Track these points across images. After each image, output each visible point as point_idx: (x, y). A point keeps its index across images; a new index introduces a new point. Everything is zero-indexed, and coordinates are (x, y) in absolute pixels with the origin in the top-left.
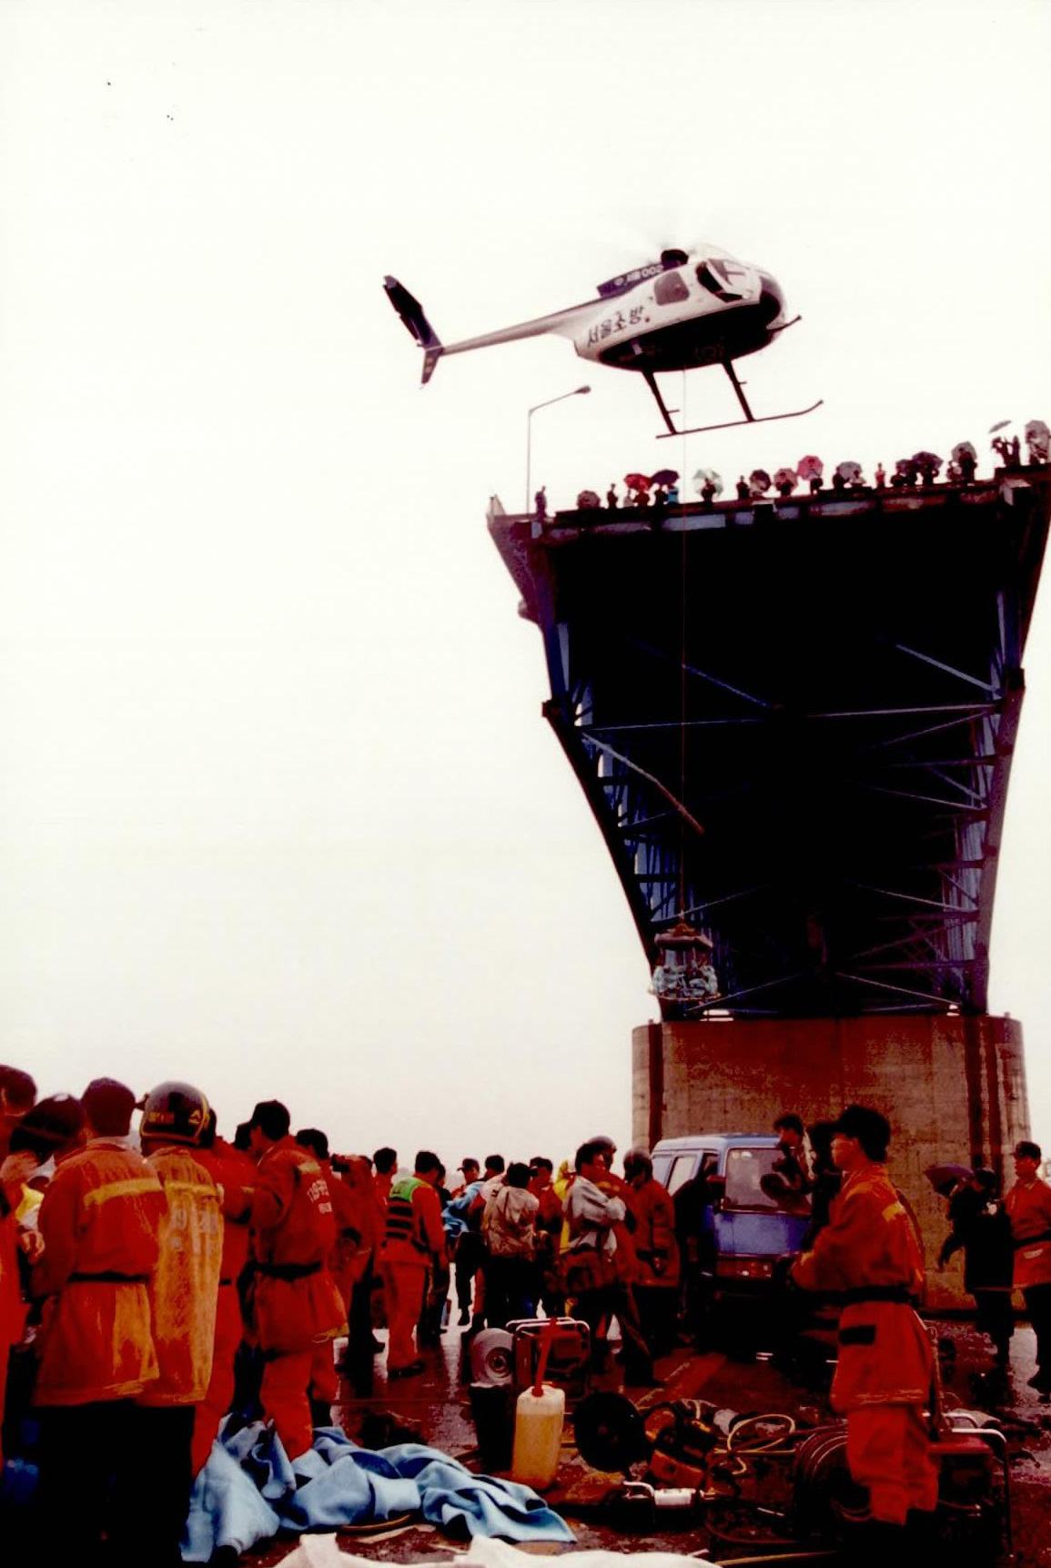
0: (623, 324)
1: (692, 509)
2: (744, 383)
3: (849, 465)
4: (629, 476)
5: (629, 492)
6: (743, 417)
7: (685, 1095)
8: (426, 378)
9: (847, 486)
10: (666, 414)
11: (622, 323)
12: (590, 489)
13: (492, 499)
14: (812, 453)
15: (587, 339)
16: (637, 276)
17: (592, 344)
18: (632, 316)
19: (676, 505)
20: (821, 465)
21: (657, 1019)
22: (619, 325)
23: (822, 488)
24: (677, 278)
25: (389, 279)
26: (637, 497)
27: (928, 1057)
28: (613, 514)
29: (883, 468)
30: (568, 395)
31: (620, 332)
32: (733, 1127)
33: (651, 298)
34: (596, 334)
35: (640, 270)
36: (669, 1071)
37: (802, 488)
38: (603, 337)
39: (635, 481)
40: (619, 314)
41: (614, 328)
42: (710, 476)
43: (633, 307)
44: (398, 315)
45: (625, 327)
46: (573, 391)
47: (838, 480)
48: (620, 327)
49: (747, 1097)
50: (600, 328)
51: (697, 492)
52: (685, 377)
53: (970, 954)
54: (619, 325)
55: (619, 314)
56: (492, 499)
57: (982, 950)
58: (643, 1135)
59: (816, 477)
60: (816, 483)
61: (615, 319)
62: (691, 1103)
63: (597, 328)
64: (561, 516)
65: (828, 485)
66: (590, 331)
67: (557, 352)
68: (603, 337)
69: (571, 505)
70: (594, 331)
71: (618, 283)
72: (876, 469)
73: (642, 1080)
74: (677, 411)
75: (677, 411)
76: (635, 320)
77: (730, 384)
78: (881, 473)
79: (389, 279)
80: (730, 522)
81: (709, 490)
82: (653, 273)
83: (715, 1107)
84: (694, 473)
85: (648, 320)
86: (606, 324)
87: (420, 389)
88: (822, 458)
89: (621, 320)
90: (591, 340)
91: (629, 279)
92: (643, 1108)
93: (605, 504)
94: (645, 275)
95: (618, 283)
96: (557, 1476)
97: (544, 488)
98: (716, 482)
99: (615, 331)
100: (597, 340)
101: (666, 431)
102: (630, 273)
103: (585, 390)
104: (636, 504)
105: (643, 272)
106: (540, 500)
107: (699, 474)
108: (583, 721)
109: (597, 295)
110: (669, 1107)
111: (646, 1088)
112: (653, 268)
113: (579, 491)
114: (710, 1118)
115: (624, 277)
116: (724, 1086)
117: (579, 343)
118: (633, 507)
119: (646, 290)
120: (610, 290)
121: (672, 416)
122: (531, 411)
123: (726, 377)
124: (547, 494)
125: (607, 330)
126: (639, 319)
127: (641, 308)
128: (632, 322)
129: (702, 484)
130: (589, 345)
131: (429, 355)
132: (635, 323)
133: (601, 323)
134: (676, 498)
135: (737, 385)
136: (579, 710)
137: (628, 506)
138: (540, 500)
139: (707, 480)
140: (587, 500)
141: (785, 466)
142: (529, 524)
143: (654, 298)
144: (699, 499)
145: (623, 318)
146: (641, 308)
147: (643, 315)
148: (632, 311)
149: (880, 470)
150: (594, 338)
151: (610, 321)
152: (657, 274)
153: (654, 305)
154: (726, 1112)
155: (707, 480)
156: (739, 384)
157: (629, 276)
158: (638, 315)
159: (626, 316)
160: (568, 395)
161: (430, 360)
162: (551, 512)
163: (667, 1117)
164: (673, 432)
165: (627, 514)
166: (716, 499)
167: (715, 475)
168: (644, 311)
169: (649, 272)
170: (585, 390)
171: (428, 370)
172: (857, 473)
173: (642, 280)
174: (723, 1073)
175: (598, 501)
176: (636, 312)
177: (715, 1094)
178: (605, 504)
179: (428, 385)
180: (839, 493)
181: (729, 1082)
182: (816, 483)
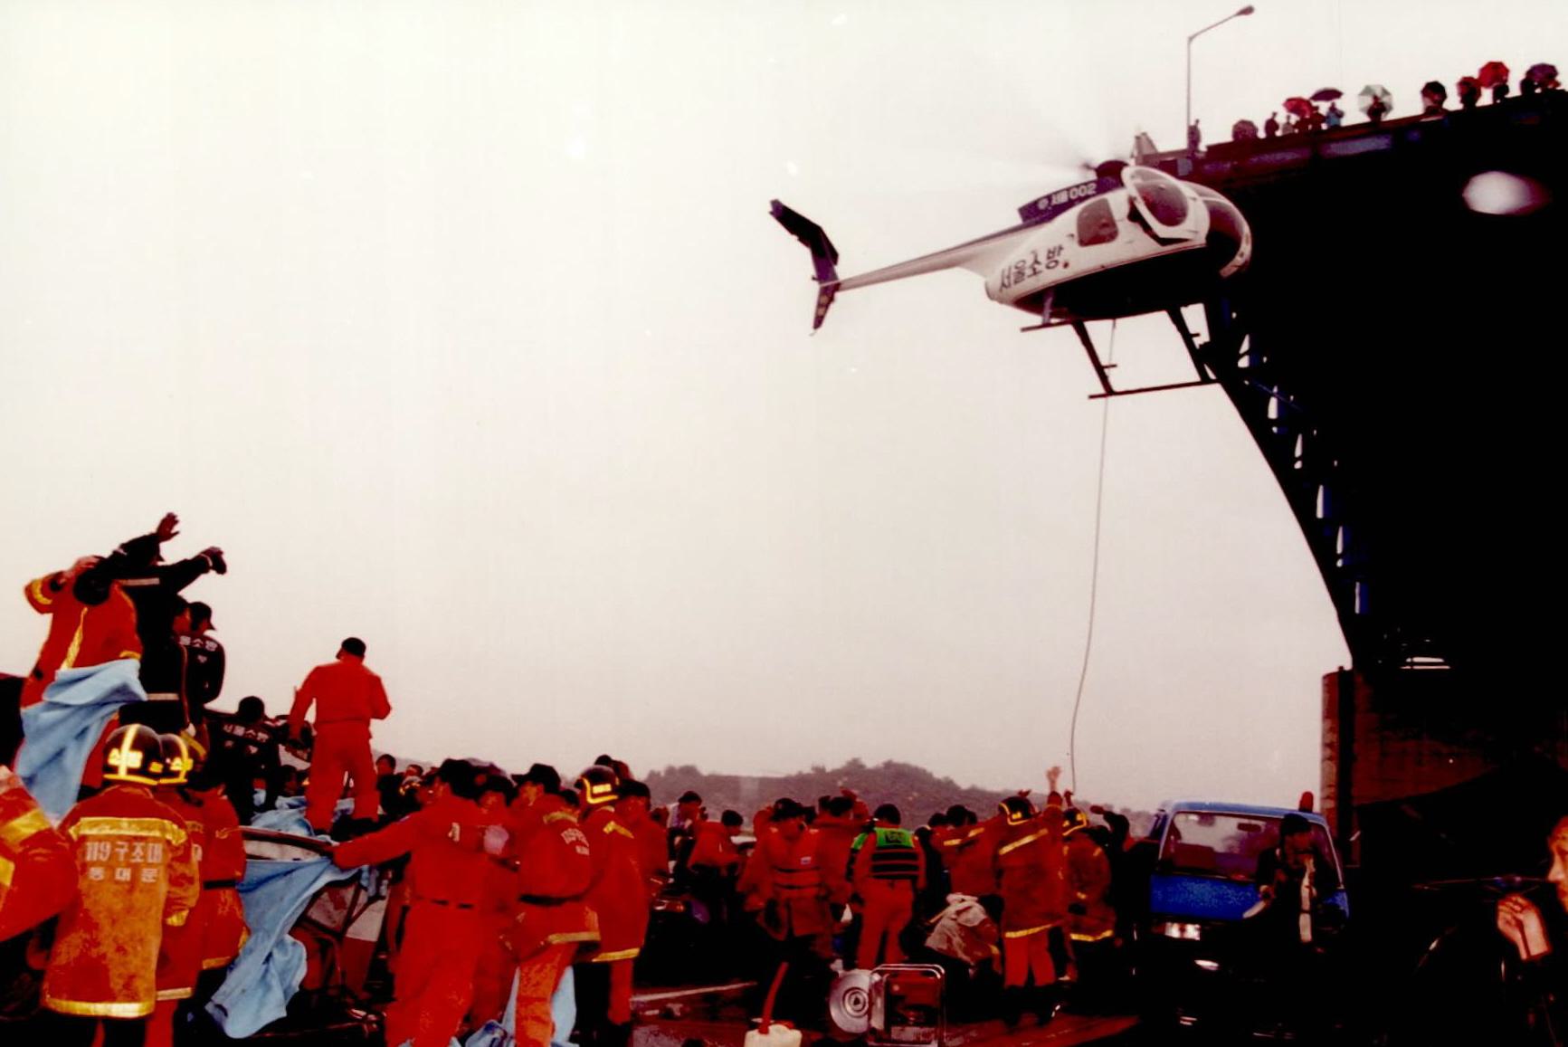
0: (1038, 267)
1: (1357, 131)
5: (1288, 117)
8: (818, 322)
10: (1100, 370)
11: (1036, 266)
13: (1138, 138)
15: (998, 284)
16: (1063, 198)
17: (1004, 289)
18: (1049, 258)
19: (1336, 129)
22: (1034, 269)
24: (1105, 204)
26: (1298, 123)
30: (1230, 18)
31: (1034, 278)
33: (1072, 236)
34: (1009, 277)
35: (1068, 190)
38: (1016, 282)
39: (1295, 105)
40: (1035, 253)
41: (1028, 272)
42: (1379, 93)
43: (1052, 245)
44: (794, 238)
45: (1040, 272)
47: (1526, 84)
48: (1035, 273)
50: (1014, 270)
51: (1362, 110)
55: (1035, 253)
61: (1030, 261)
63: (1010, 269)
64: (1213, 149)
66: (1003, 272)
67: (966, 286)
69: (1227, 137)
70: (1006, 273)
71: (1042, 206)
74: (1092, 397)
75: (1092, 397)
76: (1053, 264)
82: (1082, 195)
84: (1361, 89)
85: (1066, 265)
86: (1019, 265)
87: (812, 335)
89: (1037, 262)
90: (1003, 285)
93: (1262, 134)
94: (1073, 197)
95: (1042, 206)
97: (1197, 121)
98: (1385, 99)
99: (1029, 276)
100: (1010, 285)
101: (1101, 390)
102: (1056, 193)
103: (1247, 11)
104: (1296, 131)
105: (1071, 192)
109: (1018, 221)
112: (1084, 187)
113: (1235, 120)
115: (1049, 197)
117: (990, 285)
118: (1294, 134)
120: (1036, 214)
122: (1191, 39)
123: (1173, 328)
124: (1201, 127)
126: (1056, 262)
127: (1061, 248)
128: (1048, 267)
129: (1369, 101)
130: (1001, 290)
132: (1053, 267)
133: (1013, 264)
137: (1288, 132)
139: (1376, 98)
140: (1243, 131)
141: (1467, 74)
142: (1175, 162)
144: (1365, 119)
145: (1040, 259)
146: (1061, 248)
147: (1061, 259)
148: (1050, 252)
150: (1006, 282)
151: (1024, 261)
152: (1087, 197)
155: (1376, 98)
157: (1054, 198)
158: (1057, 258)
159: (1042, 258)
160: (1230, 18)
161: (825, 299)
162: (1202, 147)
164: (1109, 392)
165: (1289, 141)
167: (1385, 92)
168: (1063, 252)
170: (1247, 11)
173: (1070, 204)
175: (1255, 130)
176: (1053, 253)
178: (1262, 134)
179: (820, 330)
182: (1501, 90)
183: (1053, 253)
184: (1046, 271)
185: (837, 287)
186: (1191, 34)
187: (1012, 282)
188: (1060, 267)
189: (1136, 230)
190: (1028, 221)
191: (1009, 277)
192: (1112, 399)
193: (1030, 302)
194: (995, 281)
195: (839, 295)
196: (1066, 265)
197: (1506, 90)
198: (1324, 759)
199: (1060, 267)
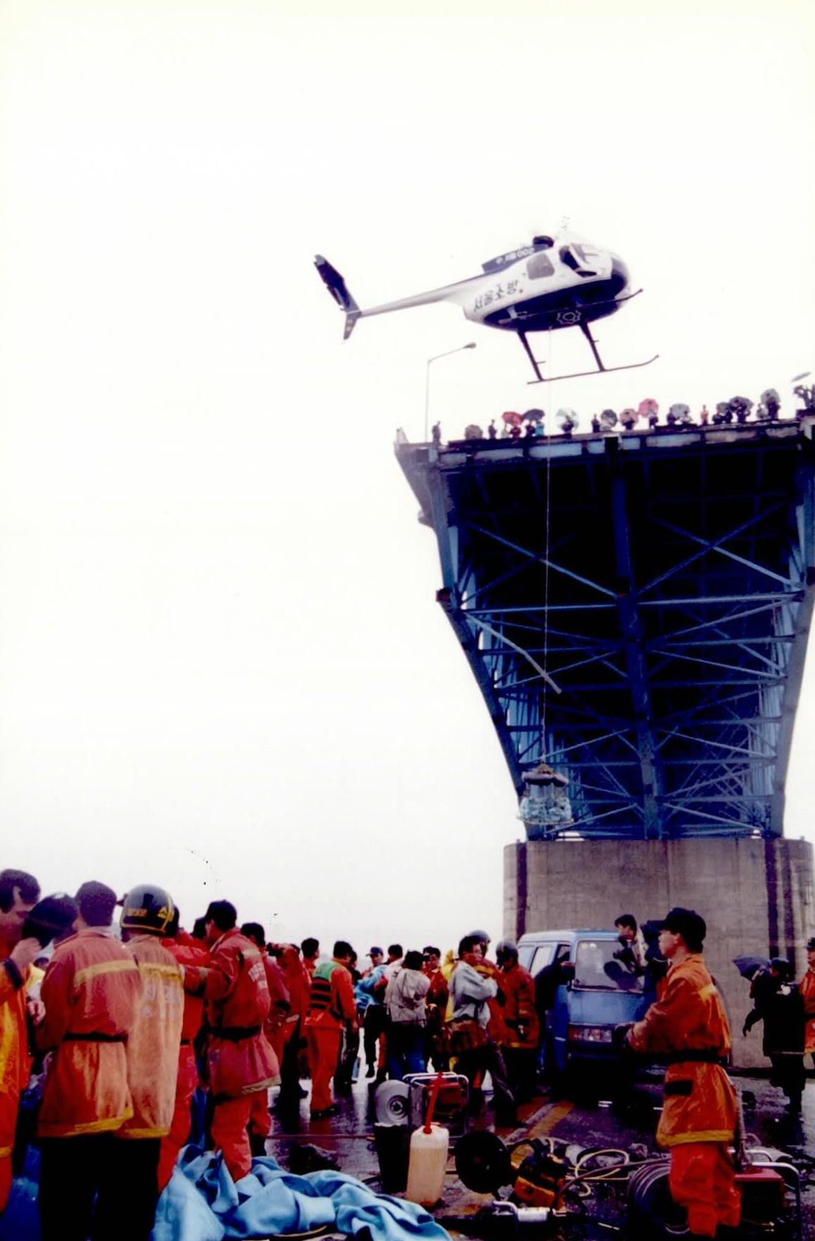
3: (680, 406)
6: (597, 368)
8: (347, 335)
10: (535, 364)
12: (475, 423)
14: (650, 396)
15: (473, 307)
16: (513, 257)
18: (509, 288)
20: (657, 406)
27: (736, 872)
28: (493, 444)
30: (459, 350)
33: (524, 274)
34: (481, 302)
35: (516, 252)
36: (531, 880)
37: (642, 425)
38: (486, 304)
39: (510, 417)
41: (495, 297)
42: (570, 414)
45: (504, 296)
47: (671, 418)
48: (500, 296)
50: (484, 297)
53: (770, 791)
56: (398, 431)
57: (780, 787)
60: (653, 421)
61: (496, 290)
63: (481, 297)
65: (663, 422)
68: (486, 304)
69: (460, 436)
71: (498, 262)
72: (701, 410)
79: (318, 257)
80: (585, 450)
81: (569, 426)
82: (525, 254)
85: (521, 291)
88: (658, 401)
89: (500, 290)
90: (477, 307)
91: (507, 258)
92: (511, 909)
94: (519, 256)
95: (498, 262)
98: (574, 419)
99: (496, 299)
100: (481, 306)
101: (535, 378)
102: (508, 254)
103: (471, 346)
106: (436, 431)
109: (481, 271)
110: (532, 908)
112: (526, 250)
113: (467, 425)
115: (503, 257)
120: (492, 267)
122: (430, 362)
124: (441, 427)
125: (489, 299)
126: (515, 290)
127: (517, 282)
128: (509, 293)
129: (563, 420)
130: (475, 310)
131: (349, 317)
135: (592, 342)
137: (505, 437)
138: (436, 431)
139: (567, 417)
140: (472, 429)
144: (561, 432)
145: (503, 289)
146: (517, 282)
147: (518, 287)
148: (509, 284)
149: (704, 411)
150: (479, 305)
151: (491, 291)
152: (529, 255)
155: (567, 417)
158: (515, 287)
159: (505, 288)
160: (459, 350)
161: (350, 321)
166: (575, 432)
167: (574, 414)
169: (523, 253)
170: (471, 346)
171: (349, 329)
172: (686, 413)
173: (518, 259)
175: (481, 433)
176: (512, 285)
177: (569, 898)
179: (347, 341)
180: (671, 429)
182: (653, 421)
183: (512, 285)
184: (507, 296)
185: (359, 315)
186: (430, 358)
187: (483, 304)
188: (517, 292)
189: (567, 270)
190: (488, 272)
191: (481, 302)
192: (542, 384)
193: (495, 319)
194: (470, 306)
195: (360, 322)
196: (521, 291)
198: (505, 910)
199: (517, 292)
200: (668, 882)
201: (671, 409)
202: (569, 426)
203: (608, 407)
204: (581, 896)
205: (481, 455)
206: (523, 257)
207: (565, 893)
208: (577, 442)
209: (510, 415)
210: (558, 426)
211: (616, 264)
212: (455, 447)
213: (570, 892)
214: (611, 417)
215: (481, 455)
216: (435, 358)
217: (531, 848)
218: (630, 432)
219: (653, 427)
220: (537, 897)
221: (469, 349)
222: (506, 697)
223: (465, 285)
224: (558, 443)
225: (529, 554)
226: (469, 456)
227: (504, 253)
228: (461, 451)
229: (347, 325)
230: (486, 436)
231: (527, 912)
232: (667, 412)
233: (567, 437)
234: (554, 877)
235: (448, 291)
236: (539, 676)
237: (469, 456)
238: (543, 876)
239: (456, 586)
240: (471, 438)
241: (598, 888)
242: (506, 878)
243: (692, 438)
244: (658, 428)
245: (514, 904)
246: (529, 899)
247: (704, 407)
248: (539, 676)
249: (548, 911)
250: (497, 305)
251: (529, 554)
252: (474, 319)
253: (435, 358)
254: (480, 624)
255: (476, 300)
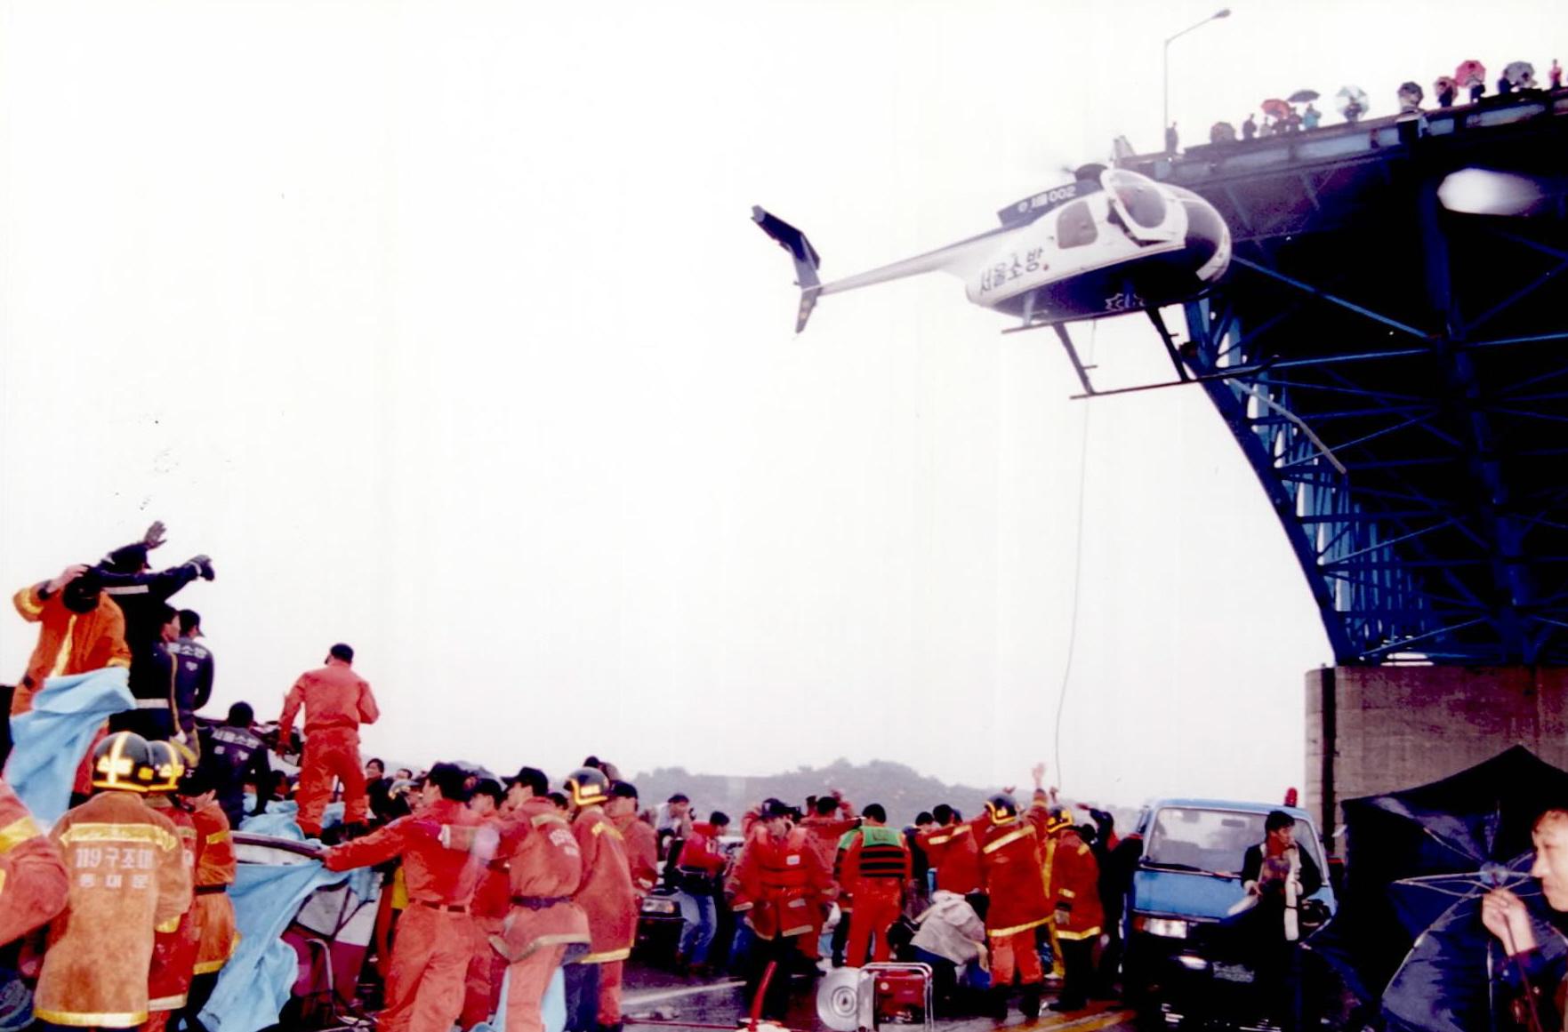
0: (1019, 270)
2: (1176, 335)
3: (1520, 65)
4: (1267, 102)
7: (1359, 739)
8: (801, 326)
9: (1515, 90)
10: (1081, 370)
11: (1017, 269)
12: (1225, 120)
13: (1116, 141)
14: (1472, 57)
16: (1043, 201)
17: (985, 293)
18: (1029, 260)
20: (1483, 70)
21: (1329, 659)
22: (1015, 272)
23: (1485, 95)
24: (1084, 209)
25: (757, 210)
28: (1250, 145)
29: (1559, 65)
31: (1015, 280)
32: (1412, 776)
33: (1052, 238)
34: (988, 280)
35: (1048, 193)
36: (1342, 717)
37: (1463, 98)
38: (996, 285)
39: (1272, 106)
40: (1014, 255)
41: (1009, 274)
42: (1355, 94)
45: (1021, 274)
46: (1210, 16)
47: (1504, 84)
48: (1016, 275)
49: (1428, 745)
50: (993, 273)
52: (1095, 327)
54: (1015, 272)
56: (1116, 141)
58: (1315, 781)
59: (1478, 84)
60: (1478, 91)
61: (1010, 264)
62: (1366, 749)
63: (990, 271)
64: (1191, 152)
65: (1492, 90)
67: (947, 289)
68: (996, 285)
69: (1204, 139)
70: (986, 277)
71: (1022, 209)
72: (1550, 67)
73: (1315, 725)
75: (1074, 398)
76: (1033, 267)
77: (1158, 337)
78: (1556, 71)
79: (757, 210)
81: (1354, 109)
82: (1061, 198)
83: (1393, 754)
84: (1338, 89)
85: (1046, 268)
86: (1000, 267)
88: (1484, 62)
89: (1017, 265)
90: (983, 288)
91: (1035, 204)
92: (1315, 754)
93: (1240, 136)
94: (1052, 200)
96: (1427, 703)
98: (1362, 100)
99: (1010, 279)
101: (1081, 390)
103: (1224, 14)
105: (1051, 195)
106: (1171, 137)
107: (1344, 92)
108: (1230, 360)
110: (1342, 753)
111: (1318, 733)
112: (1063, 190)
114: (1387, 765)
115: (1029, 200)
116: (1403, 734)
119: (1049, 223)
120: (1015, 217)
121: (1088, 372)
122: (1168, 42)
123: (1152, 328)
125: (1000, 277)
126: (1037, 264)
128: (1028, 270)
129: (1345, 102)
130: (981, 293)
131: (806, 296)
132: (1033, 270)
134: (1316, 122)
136: (1225, 346)
138: (1171, 137)
139: (1352, 99)
140: (1221, 130)
143: (1056, 238)
144: (1342, 119)
146: (1041, 251)
147: (1042, 261)
148: (1030, 254)
149: (1555, 68)
150: (986, 284)
151: (1004, 264)
152: (1067, 200)
153: (1054, 246)
154: (1403, 760)
155: (1352, 99)
156: (1170, 336)
157: (1034, 200)
158: (1037, 260)
159: (1023, 261)
161: (807, 304)
162: (1180, 149)
163: (1339, 763)
164: (1092, 393)
166: (1363, 118)
167: (1362, 93)
169: (1058, 196)
170: (1224, 14)
171: (804, 316)
172: (1526, 76)
174: (1402, 720)
175: (1233, 131)
177: (1393, 741)
179: (802, 334)
180: (1506, 97)
181: (1408, 730)
182: (1478, 91)
183: (1033, 255)
185: (819, 292)
191: (988, 280)
194: (975, 284)
195: (820, 299)
196: (1046, 268)
197: (1481, 89)
198: (1308, 755)
200: (1536, 722)
201: (1506, 72)
202: (1354, 109)
203: (1408, 80)
204: (1410, 739)
205: (1231, 162)
206: (1061, 202)
207: (1388, 734)
208: (1362, 132)
209: (1274, 104)
210: (1339, 110)
211: (832, 791)
212: (1195, 153)
213: (1395, 733)
214: (1413, 92)
215: (1231, 162)
216: (1174, 38)
217: (1340, 676)
218: (1447, 109)
219: (1476, 100)
220: (1349, 739)
221: (1220, 20)
222: (1290, 479)
223: (962, 249)
224: (1337, 137)
225: (1307, 288)
226: (1214, 165)
227: (1030, 194)
228: (1204, 160)
229: (802, 310)
230: (1240, 136)
231: (1336, 759)
232: (1499, 76)
233: (1351, 127)
234: (1373, 712)
235: (942, 256)
236: (1333, 449)
237: (1214, 165)
238: (1358, 711)
239: (1209, 339)
240: (1219, 139)
241: (1434, 729)
242: (1310, 711)
243: (1534, 109)
244: (1482, 100)
245: (1319, 748)
246: (1338, 742)
247: (1555, 62)
248: (1333, 449)
249: (1364, 758)
250: (1011, 287)
251: (1307, 288)
252: (982, 304)
253: (1174, 38)
254: (1245, 387)
255: (983, 277)
